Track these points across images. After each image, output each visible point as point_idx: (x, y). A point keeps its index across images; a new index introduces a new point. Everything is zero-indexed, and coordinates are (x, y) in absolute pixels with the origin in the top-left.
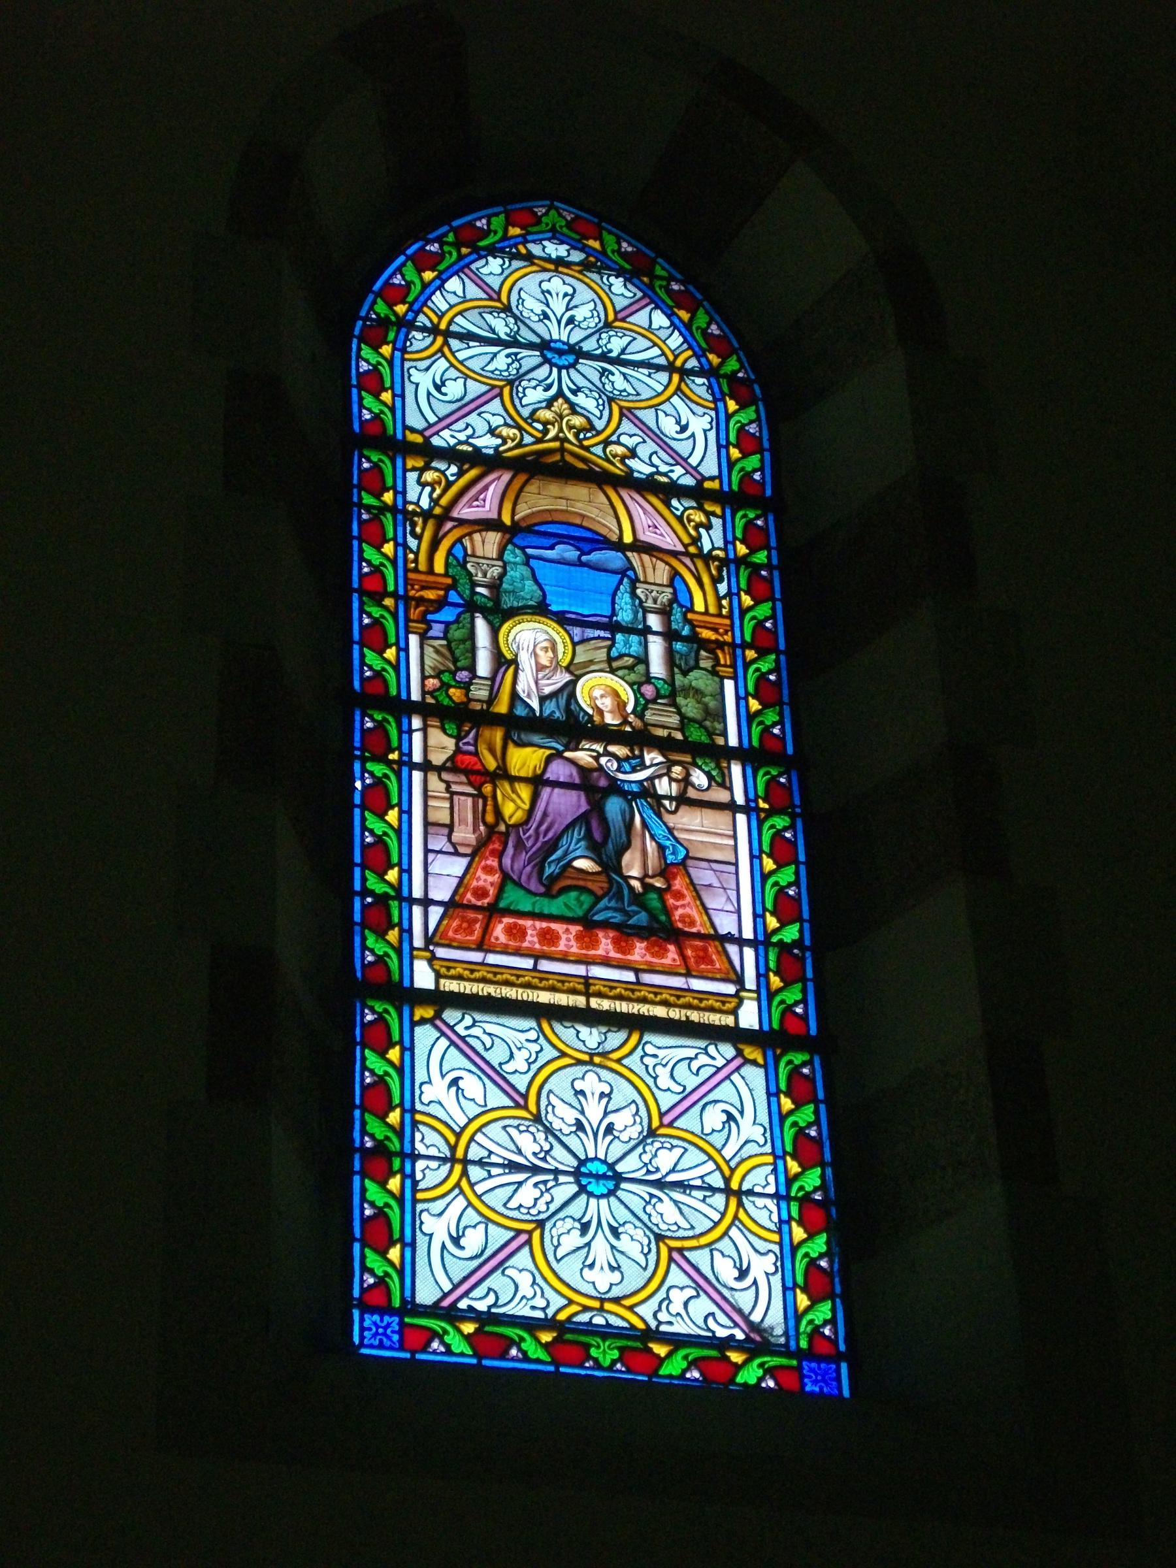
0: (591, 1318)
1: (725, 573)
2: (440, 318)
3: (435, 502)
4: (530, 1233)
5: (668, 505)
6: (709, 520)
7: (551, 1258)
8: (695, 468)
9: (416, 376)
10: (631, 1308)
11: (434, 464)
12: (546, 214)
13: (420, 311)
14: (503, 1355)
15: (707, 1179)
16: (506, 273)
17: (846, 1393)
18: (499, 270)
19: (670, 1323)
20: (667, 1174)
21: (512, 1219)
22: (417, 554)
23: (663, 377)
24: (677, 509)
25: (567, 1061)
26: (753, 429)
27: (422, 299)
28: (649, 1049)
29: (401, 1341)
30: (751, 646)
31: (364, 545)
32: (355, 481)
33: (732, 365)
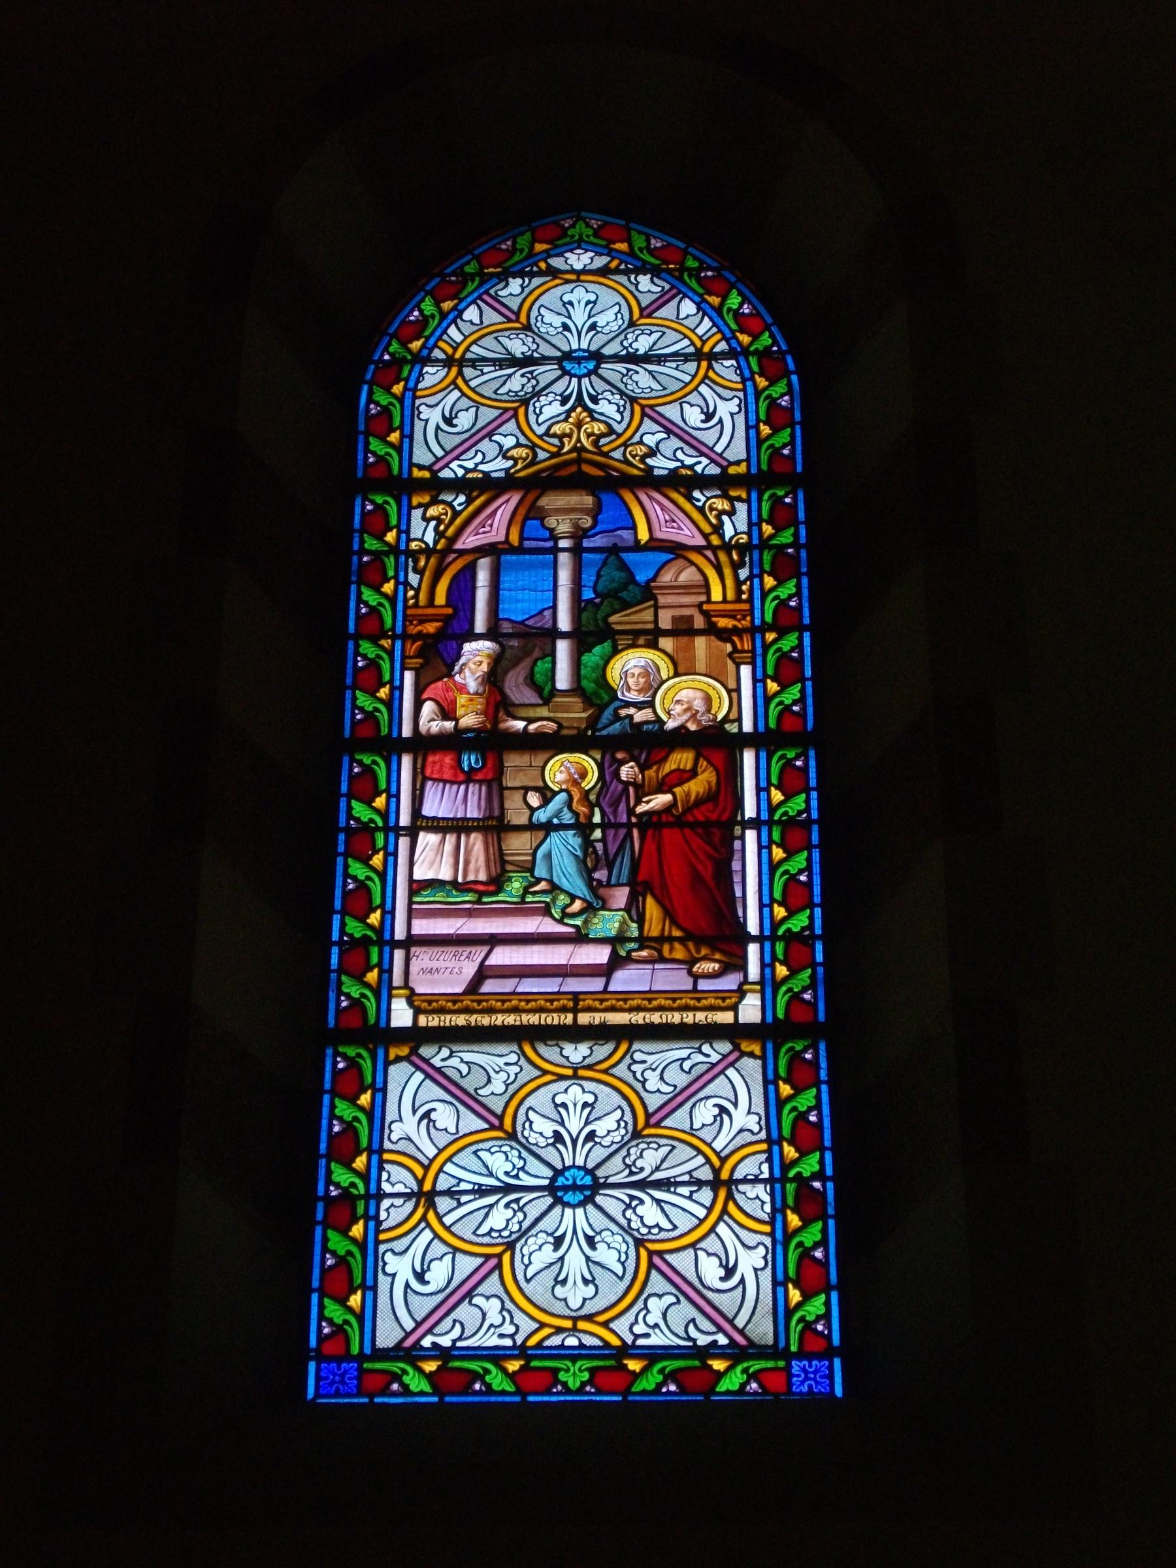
0: (563, 1341)
1: (747, 559)
2: (455, 349)
3: (439, 535)
4: (499, 1256)
5: (690, 498)
6: (733, 506)
7: (520, 1277)
8: (721, 455)
9: (425, 412)
10: (605, 1325)
11: (441, 497)
12: (573, 226)
13: (435, 346)
14: (467, 1390)
15: (695, 1174)
16: (527, 291)
17: (839, 1391)
18: (502, 1088)
19: (647, 1335)
20: (652, 1173)
21: (482, 1245)
22: (417, 591)
23: (691, 367)
24: (698, 500)
25: (548, 1078)
26: (784, 402)
27: (437, 333)
28: (638, 1056)
29: (359, 1386)
30: (771, 628)
31: (327, 1301)
32: (327, 1086)
33: (766, 340)
